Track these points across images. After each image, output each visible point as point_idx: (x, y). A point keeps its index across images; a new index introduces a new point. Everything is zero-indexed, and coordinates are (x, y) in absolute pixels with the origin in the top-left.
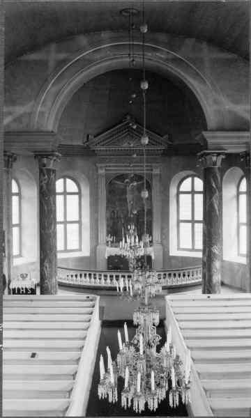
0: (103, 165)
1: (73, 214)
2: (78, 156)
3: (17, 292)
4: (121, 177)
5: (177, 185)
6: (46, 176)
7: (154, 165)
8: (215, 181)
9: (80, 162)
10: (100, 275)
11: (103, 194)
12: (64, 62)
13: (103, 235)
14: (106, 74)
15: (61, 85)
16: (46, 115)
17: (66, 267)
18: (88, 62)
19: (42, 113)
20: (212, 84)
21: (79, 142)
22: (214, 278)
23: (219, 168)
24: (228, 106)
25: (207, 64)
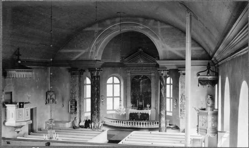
0: (130, 71)
1: (117, 93)
2: (112, 68)
3: (224, 137)
4: (138, 77)
5: (199, 71)
6: (93, 79)
7: (152, 71)
8: (162, 82)
9: (119, 70)
10: (153, 123)
11: (129, 83)
12: (100, 31)
13: (130, 104)
14: (111, 41)
15: (100, 40)
16: (94, 53)
17: (112, 118)
18: (110, 31)
19: (92, 53)
20: (162, 40)
21: (118, 61)
22: (161, 125)
23: (164, 76)
24: (169, 48)
25: (160, 31)
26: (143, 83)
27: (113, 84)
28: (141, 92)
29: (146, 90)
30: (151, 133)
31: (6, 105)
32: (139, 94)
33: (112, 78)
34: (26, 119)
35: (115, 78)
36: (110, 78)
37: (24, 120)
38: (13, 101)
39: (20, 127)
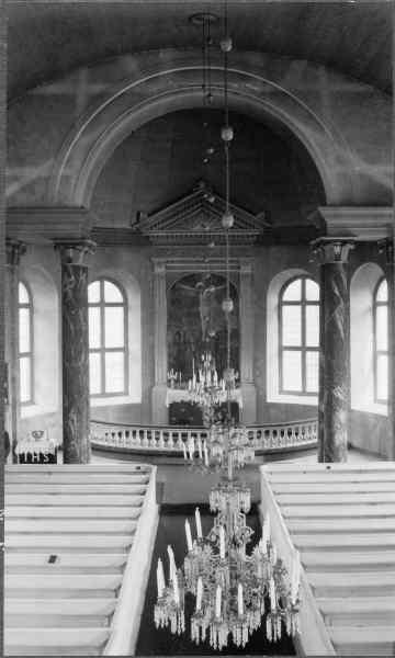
0: (162, 260)
2: (123, 245)
3: (26, 459)
4: (191, 279)
5: (278, 291)
6: (73, 278)
7: (242, 259)
8: (338, 285)
9: (126, 255)
10: (158, 433)
11: (162, 305)
12: (101, 97)
13: (162, 370)
14: (167, 117)
15: (96, 134)
16: (73, 181)
17: (103, 420)
18: (138, 98)
19: (66, 178)
20: (334, 132)
21: (124, 224)
22: (336, 437)
23: (344, 264)
24: (359, 166)
25: (326, 101)
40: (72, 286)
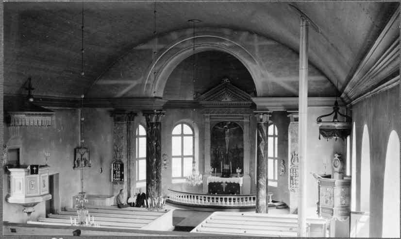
0: (209, 115)
2: (181, 109)
3: (361, 222)
4: (222, 124)
5: (320, 115)
6: (150, 128)
7: (244, 115)
8: (261, 133)
9: (191, 112)
10: (246, 198)
11: (208, 135)
12: (162, 50)
13: (209, 168)
14: (179, 66)
15: (160, 65)
16: (151, 86)
17: (180, 190)
18: (177, 50)
19: (148, 85)
20: (261, 64)
21: (190, 98)
22: (260, 201)
23: (264, 123)
24: (271, 78)
25: (257, 50)
26: (230, 134)
27: (182, 135)
28: (227, 148)
29: (235, 145)
30: (243, 214)
31: (10, 170)
32: (223, 152)
33: (180, 125)
34: (43, 192)
35: (185, 126)
36: (178, 126)
37: (38, 194)
38: (22, 163)
39: (33, 204)
40: (150, 131)
